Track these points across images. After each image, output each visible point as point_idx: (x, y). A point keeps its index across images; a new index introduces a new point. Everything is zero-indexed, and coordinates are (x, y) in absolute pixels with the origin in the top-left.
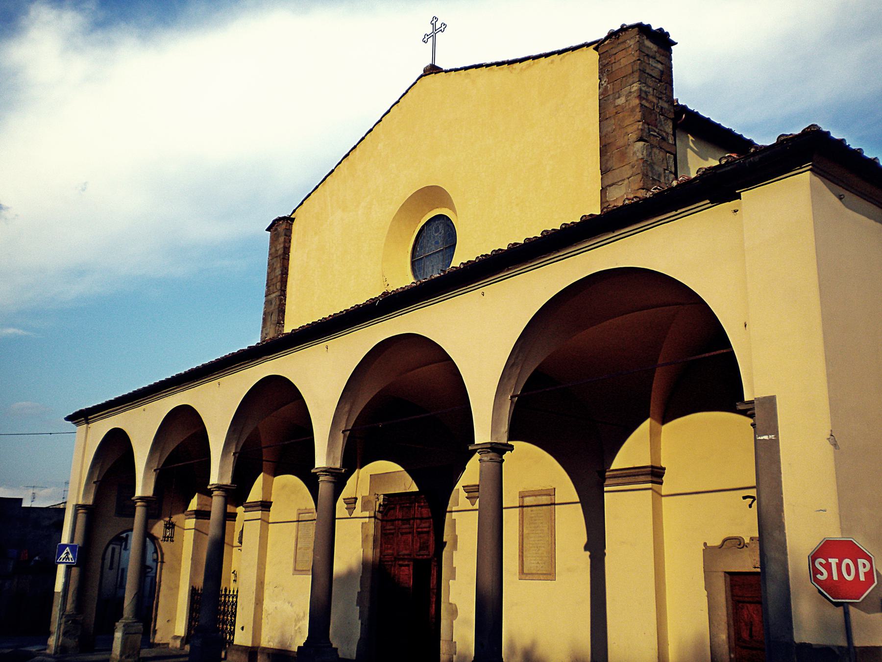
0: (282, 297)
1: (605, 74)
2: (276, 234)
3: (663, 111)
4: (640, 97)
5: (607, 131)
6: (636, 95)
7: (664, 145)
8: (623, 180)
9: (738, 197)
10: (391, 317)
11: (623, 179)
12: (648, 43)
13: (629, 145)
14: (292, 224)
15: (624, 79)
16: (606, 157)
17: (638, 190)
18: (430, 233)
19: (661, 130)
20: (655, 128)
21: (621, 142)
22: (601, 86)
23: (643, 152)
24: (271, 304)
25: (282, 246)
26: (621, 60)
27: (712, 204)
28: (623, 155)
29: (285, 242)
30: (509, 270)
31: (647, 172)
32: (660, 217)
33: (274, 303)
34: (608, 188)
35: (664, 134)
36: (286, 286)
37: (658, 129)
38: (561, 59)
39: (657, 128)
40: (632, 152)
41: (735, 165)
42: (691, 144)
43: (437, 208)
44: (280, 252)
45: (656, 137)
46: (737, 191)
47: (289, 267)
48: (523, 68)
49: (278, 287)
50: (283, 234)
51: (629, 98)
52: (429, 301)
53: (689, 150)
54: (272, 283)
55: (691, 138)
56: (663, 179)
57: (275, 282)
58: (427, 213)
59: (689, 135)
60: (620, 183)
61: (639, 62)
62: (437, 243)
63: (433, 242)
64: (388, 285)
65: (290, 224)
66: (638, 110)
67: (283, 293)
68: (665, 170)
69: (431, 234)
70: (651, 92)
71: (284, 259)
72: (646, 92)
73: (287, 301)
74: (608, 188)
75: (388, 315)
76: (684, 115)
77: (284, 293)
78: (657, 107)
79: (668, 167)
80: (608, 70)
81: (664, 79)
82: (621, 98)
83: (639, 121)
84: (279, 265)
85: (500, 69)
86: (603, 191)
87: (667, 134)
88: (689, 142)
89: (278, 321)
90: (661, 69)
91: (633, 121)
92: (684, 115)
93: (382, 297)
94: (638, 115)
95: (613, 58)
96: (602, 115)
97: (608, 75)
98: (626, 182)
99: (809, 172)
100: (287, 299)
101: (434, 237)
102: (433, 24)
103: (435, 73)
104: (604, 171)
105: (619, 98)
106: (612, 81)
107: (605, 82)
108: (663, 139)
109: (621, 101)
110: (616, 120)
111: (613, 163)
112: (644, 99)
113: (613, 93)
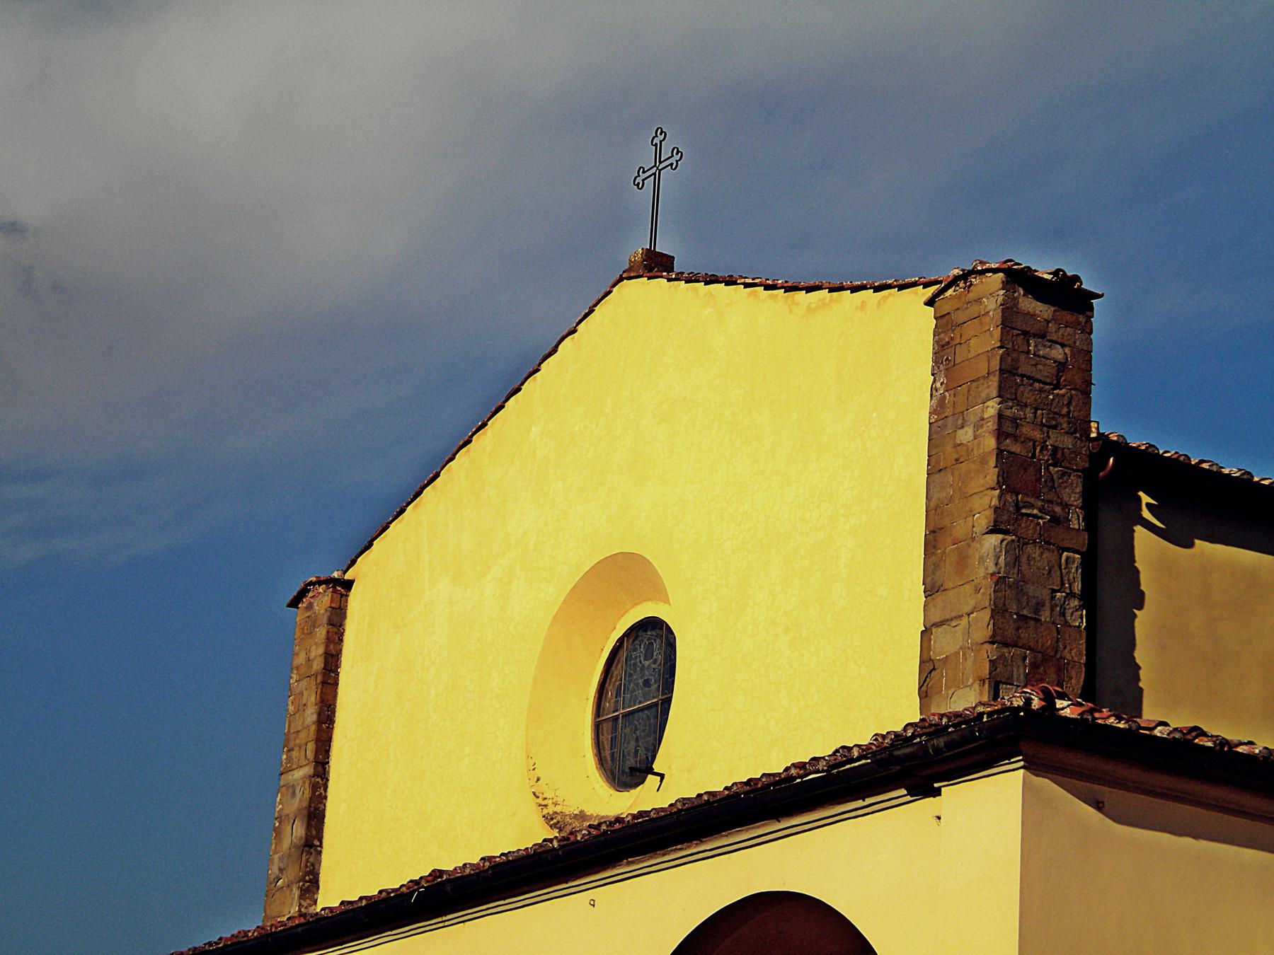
0: (319, 780)
1: (942, 367)
2: (309, 617)
3: (1059, 455)
4: (1000, 434)
5: (939, 499)
6: (991, 427)
7: (1058, 534)
8: (960, 617)
9: (937, 793)
10: (447, 923)
11: (960, 614)
12: (1029, 304)
13: (973, 539)
14: (347, 596)
15: (974, 385)
16: (933, 559)
17: (983, 644)
18: (636, 657)
19: (1051, 502)
20: (1032, 500)
21: (960, 529)
22: (934, 391)
23: (999, 558)
24: (294, 794)
25: (321, 650)
26: (972, 342)
27: (911, 797)
28: (963, 561)
29: (329, 640)
30: (629, 864)
31: (1004, 604)
32: (842, 806)
33: (299, 794)
34: (934, 630)
35: (1058, 509)
36: (327, 752)
37: (1043, 500)
38: (879, 304)
39: (1038, 497)
40: (977, 557)
41: (916, 748)
42: (1146, 514)
43: (649, 600)
44: (318, 665)
45: (1035, 516)
46: (936, 785)
47: (338, 704)
48: (813, 306)
49: (310, 755)
50: (325, 620)
51: (980, 431)
52: (507, 901)
53: (1139, 530)
54: (298, 741)
55: (1146, 499)
56: (1048, 613)
57: (304, 742)
58: (628, 611)
59: (1141, 494)
60: (954, 623)
61: (1001, 351)
62: (647, 683)
63: (641, 681)
64: (538, 780)
65: (342, 595)
66: (993, 462)
67: (320, 769)
68: (1054, 591)
69: (638, 660)
70: (1030, 415)
71: (324, 683)
72: (1014, 420)
73: (329, 789)
74: (934, 630)
75: (440, 919)
76: (1111, 460)
77: (325, 769)
78: (1044, 448)
79: (1063, 584)
80: (947, 359)
81: (1065, 380)
82: (966, 429)
83: (993, 489)
84: (313, 699)
85: (769, 296)
86: (925, 633)
87: (1066, 506)
88: (1141, 509)
89: (307, 840)
90: (1060, 357)
91: (983, 486)
92: (1111, 460)
93: (427, 882)
94: (992, 474)
95: (958, 331)
96: (933, 459)
97: (947, 369)
98: (964, 621)
99: (1022, 771)
100: (330, 784)
101: (643, 669)
102: (656, 145)
103: (649, 278)
104: (932, 589)
105: (963, 427)
106: (953, 386)
107: (942, 384)
108: (1055, 520)
109: (965, 435)
110: (957, 478)
111: (947, 574)
112: (1008, 435)
113: (954, 414)
